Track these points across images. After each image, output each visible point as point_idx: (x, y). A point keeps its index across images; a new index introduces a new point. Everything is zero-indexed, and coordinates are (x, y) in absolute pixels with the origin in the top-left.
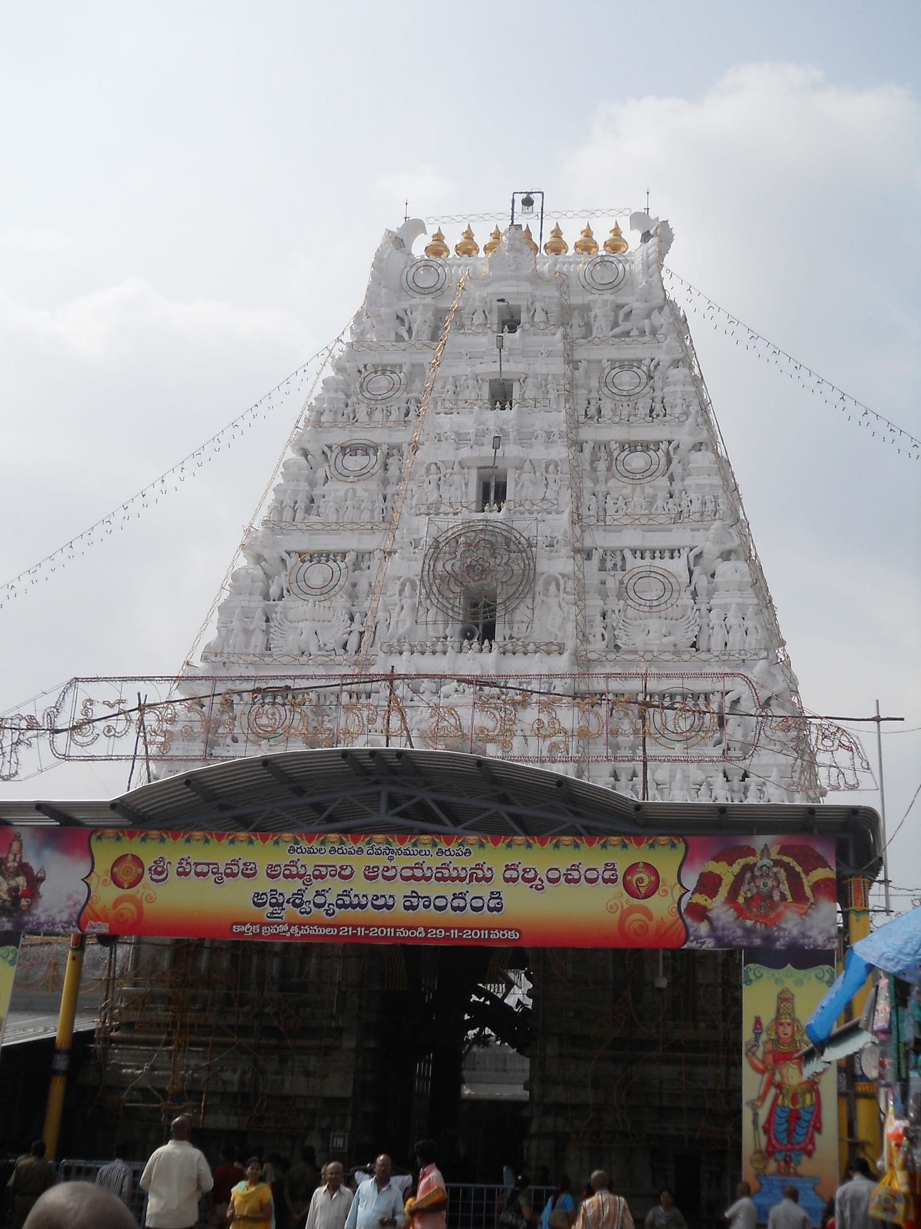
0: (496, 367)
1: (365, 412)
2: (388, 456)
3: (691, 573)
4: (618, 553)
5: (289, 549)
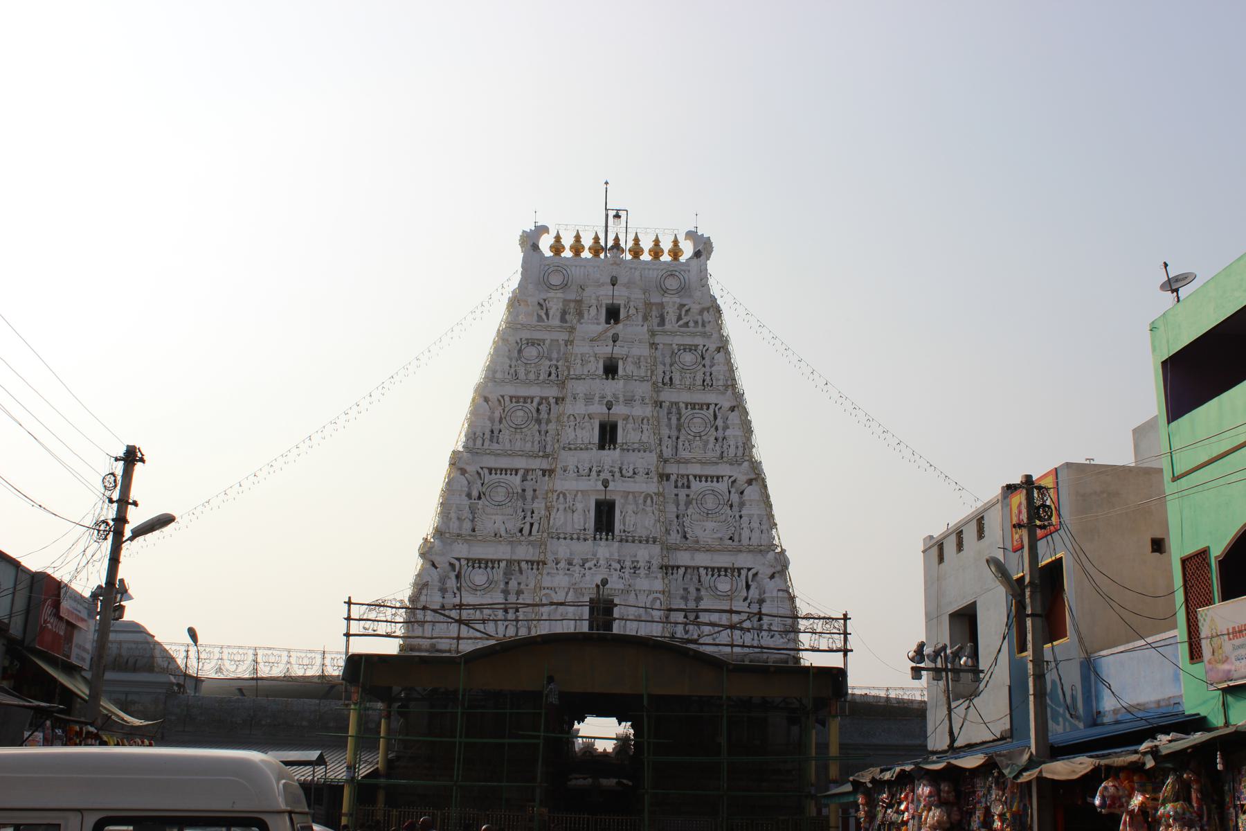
0: (609, 349)
2: (539, 404)
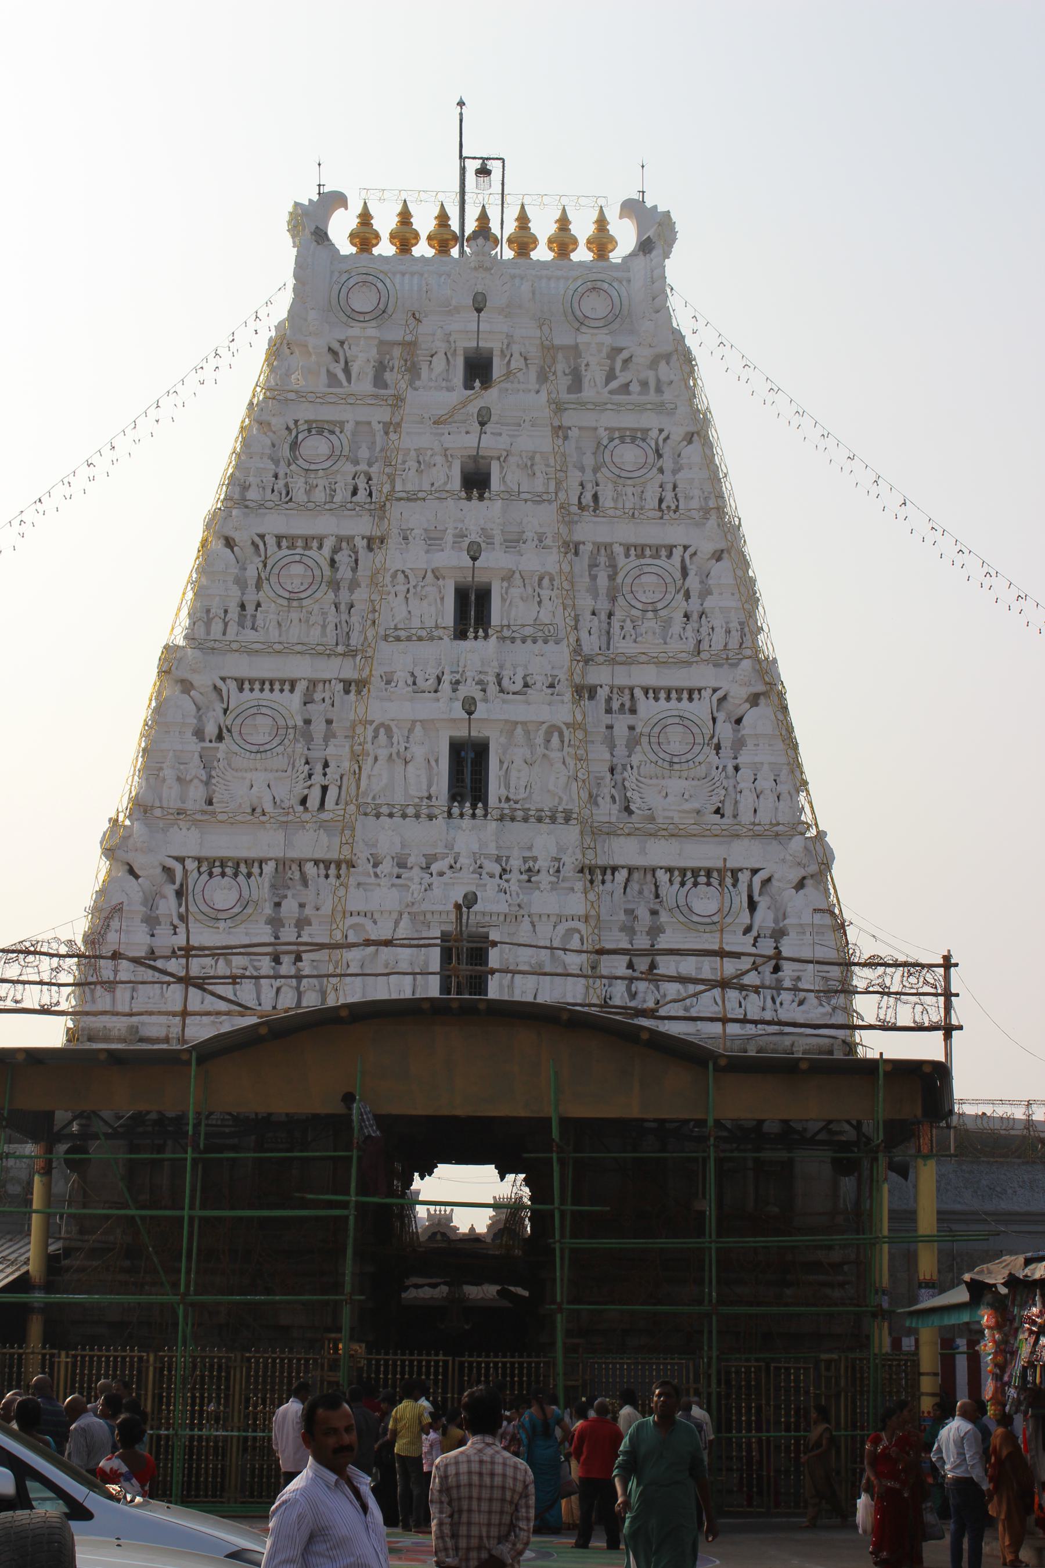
0: (471, 441)
1: (302, 490)
2: (336, 550)
3: (714, 720)
4: (627, 692)
5: (223, 675)
